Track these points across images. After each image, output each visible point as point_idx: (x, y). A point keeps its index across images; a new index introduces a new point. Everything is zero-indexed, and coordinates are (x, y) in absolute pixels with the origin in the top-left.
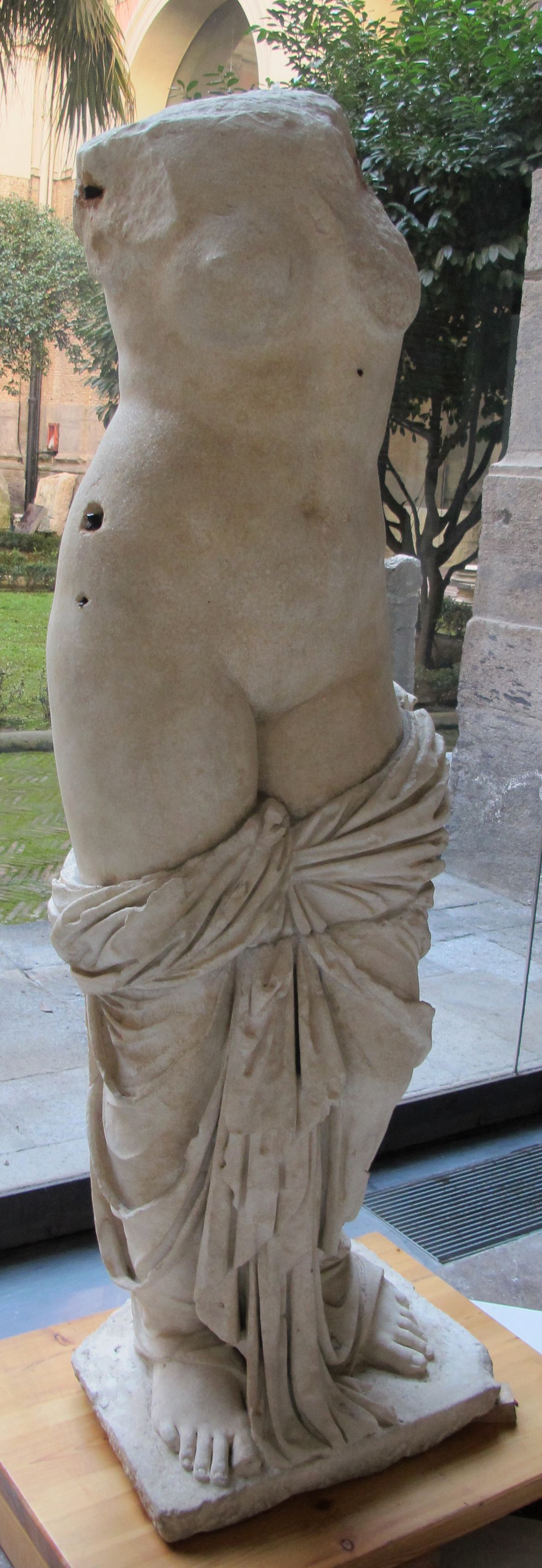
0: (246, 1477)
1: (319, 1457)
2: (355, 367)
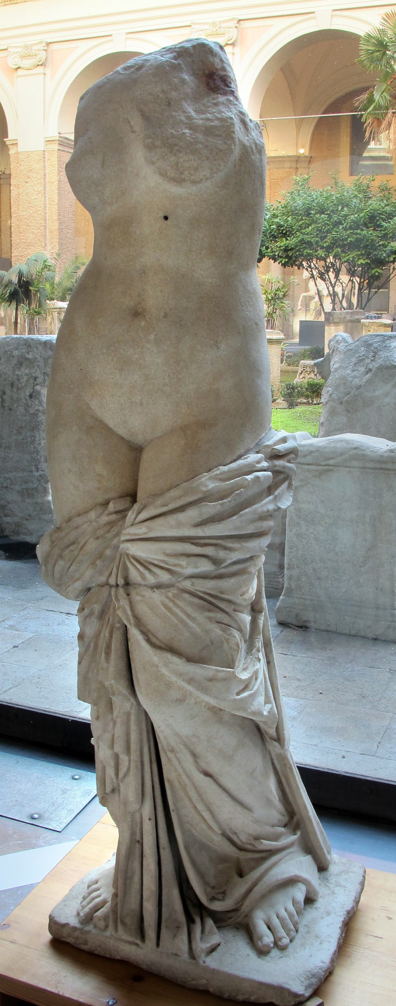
0: (95, 927)
1: (137, 945)
2: (162, 214)
